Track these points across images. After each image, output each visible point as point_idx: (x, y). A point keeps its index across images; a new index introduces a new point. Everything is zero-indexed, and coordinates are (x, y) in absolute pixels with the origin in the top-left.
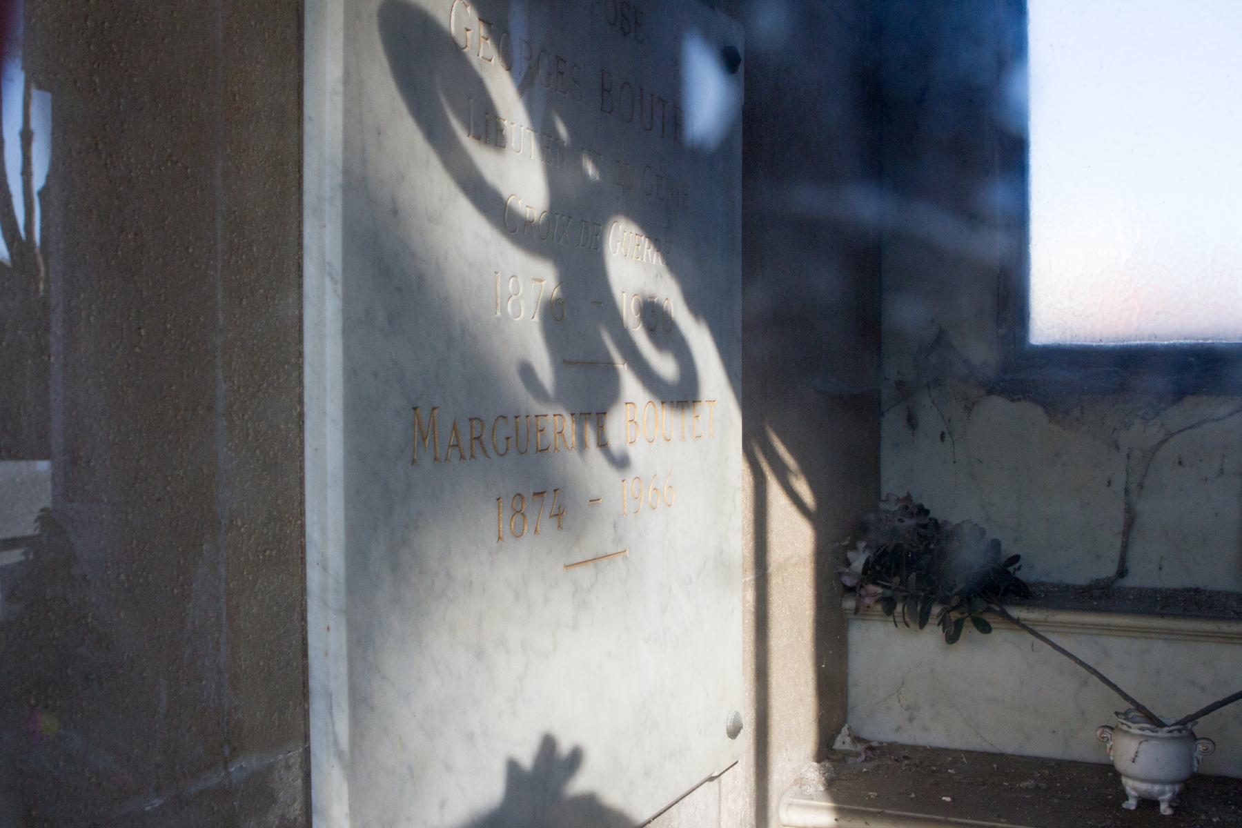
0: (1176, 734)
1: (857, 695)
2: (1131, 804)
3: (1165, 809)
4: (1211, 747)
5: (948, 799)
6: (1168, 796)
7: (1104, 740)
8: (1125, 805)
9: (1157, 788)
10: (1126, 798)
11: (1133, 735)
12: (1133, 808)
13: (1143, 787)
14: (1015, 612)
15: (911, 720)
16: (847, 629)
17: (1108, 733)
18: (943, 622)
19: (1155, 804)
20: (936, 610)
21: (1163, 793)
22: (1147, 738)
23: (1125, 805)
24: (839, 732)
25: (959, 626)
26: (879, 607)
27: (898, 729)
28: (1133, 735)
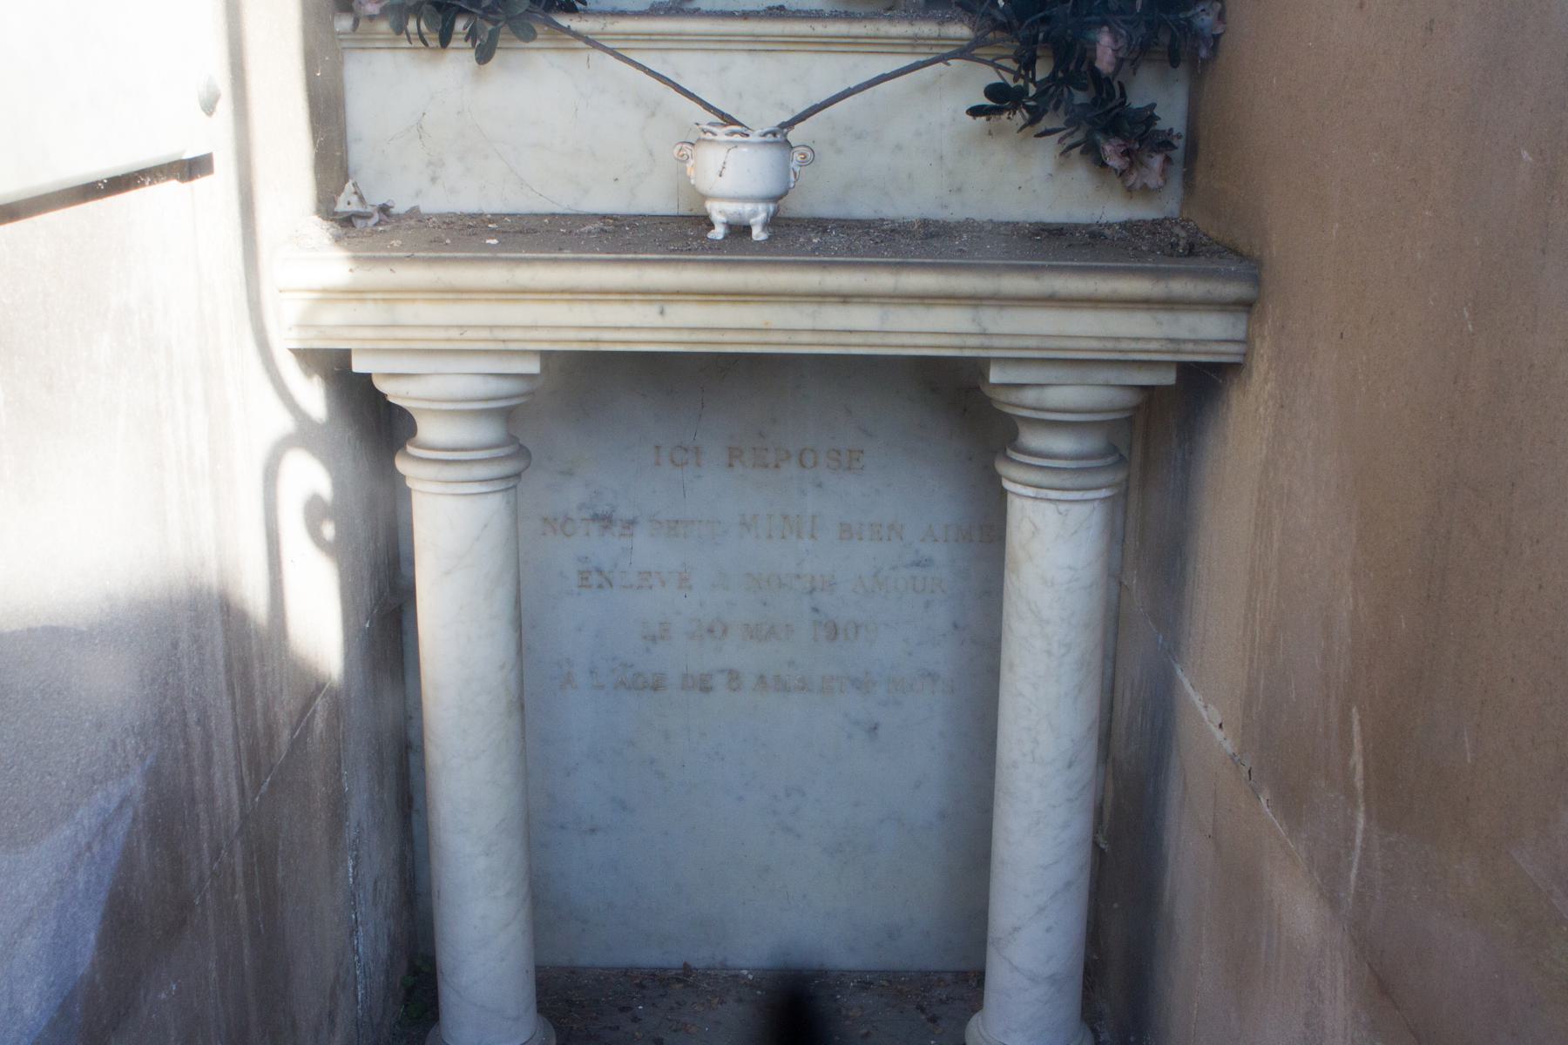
0: (770, 138)
1: (359, 155)
2: (718, 233)
3: (758, 234)
4: (809, 154)
5: (494, 241)
6: (762, 217)
7: (683, 160)
8: (710, 235)
9: (748, 208)
10: (711, 226)
11: (719, 143)
12: (720, 237)
13: (733, 208)
14: (564, 21)
15: (434, 180)
16: (342, 63)
17: (687, 150)
18: (472, 35)
19: (747, 229)
20: (460, 25)
21: (755, 214)
22: (736, 145)
23: (710, 235)
24: (341, 776)
25: (493, 37)
26: (384, 26)
27: (418, 193)
28: (719, 143)
